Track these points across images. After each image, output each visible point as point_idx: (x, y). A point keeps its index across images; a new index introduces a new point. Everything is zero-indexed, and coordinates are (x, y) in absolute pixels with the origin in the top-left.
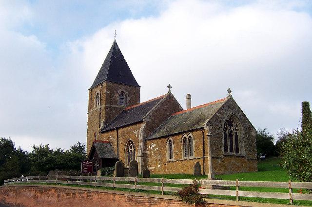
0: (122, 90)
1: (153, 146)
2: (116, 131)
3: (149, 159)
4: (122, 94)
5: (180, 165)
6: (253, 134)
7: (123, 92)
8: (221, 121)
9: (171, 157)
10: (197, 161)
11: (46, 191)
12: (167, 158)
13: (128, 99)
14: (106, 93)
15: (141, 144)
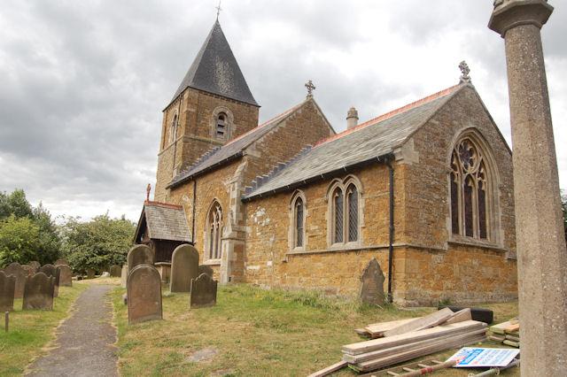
0: (221, 110)
2: (193, 183)
8: (443, 145)
10: (372, 256)
12: (328, 240)
13: (234, 128)
14: (188, 112)
15: (234, 208)
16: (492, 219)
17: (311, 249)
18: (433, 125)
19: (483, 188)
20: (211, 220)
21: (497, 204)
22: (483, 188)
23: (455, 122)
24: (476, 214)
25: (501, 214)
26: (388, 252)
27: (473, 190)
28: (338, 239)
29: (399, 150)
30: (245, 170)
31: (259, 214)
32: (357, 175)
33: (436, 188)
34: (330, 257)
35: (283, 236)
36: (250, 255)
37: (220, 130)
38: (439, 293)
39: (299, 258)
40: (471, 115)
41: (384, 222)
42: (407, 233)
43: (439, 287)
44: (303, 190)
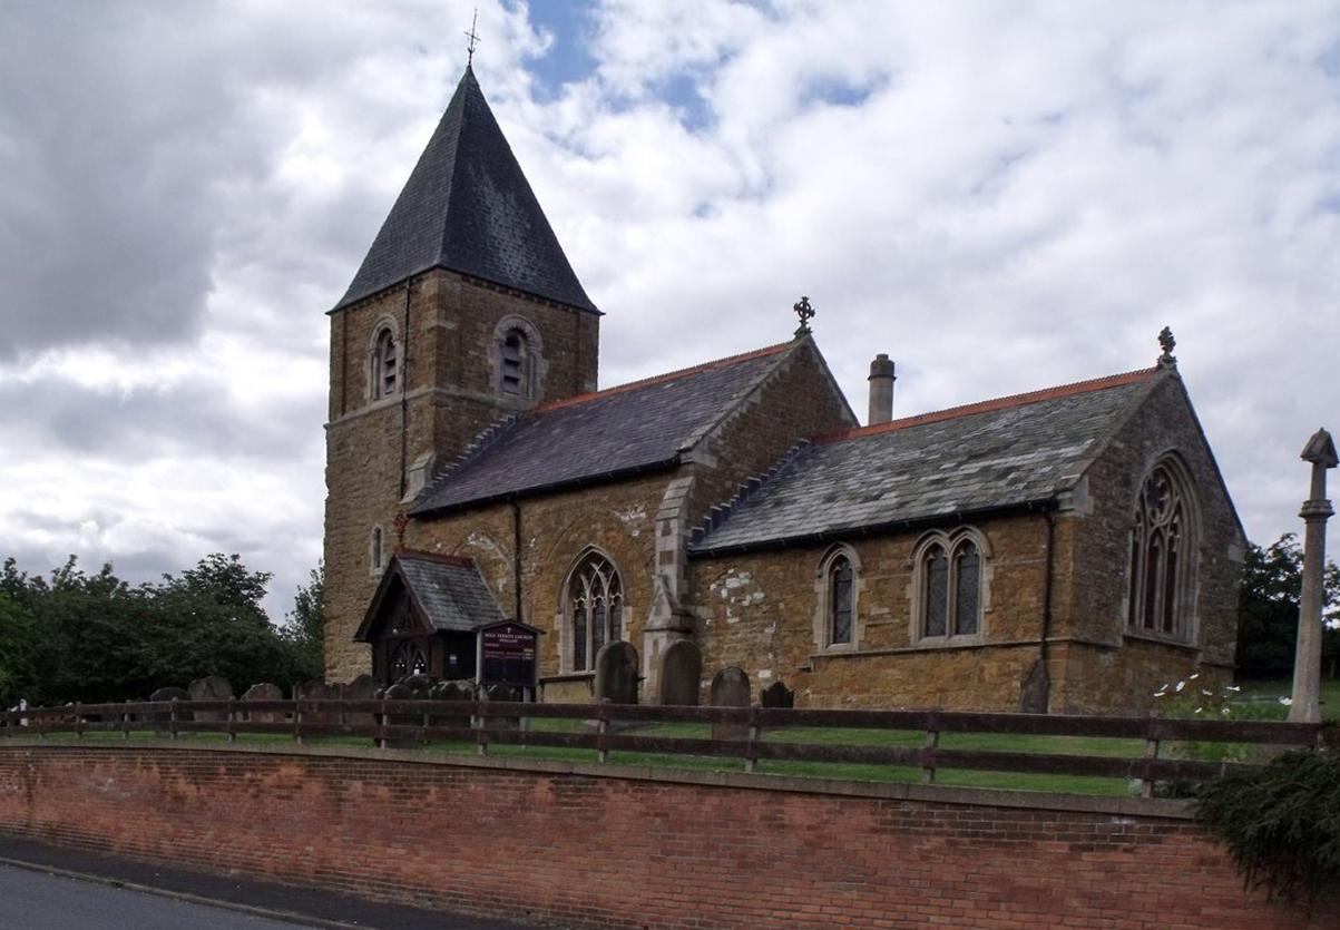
0: (513, 323)
1: (732, 583)
3: (711, 643)
4: (514, 339)
5: (893, 673)
6: (1234, 554)
7: (518, 331)
8: (1127, 482)
9: (838, 635)
11: (234, 771)
12: (913, 631)
15: (671, 571)
16: (1183, 599)
17: (873, 647)
18: (1116, 450)
19: (1175, 550)
20: (577, 590)
21: (1194, 575)
22: (1175, 550)
23: (1148, 443)
24: (1161, 593)
25: (1198, 592)
26: (1038, 649)
27: (1161, 552)
28: (927, 631)
29: (1068, 495)
30: (691, 496)
31: (732, 583)
32: (978, 527)
33: (1112, 554)
34: (917, 659)
35: (801, 624)
36: (709, 660)
37: (511, 372)
38: (1104, 709)
39: (843, 662)
40: (1170, 428)
41: (1031, 606)
42: (1071, 622)
43: (1105, 702)
44: (852, 544)
